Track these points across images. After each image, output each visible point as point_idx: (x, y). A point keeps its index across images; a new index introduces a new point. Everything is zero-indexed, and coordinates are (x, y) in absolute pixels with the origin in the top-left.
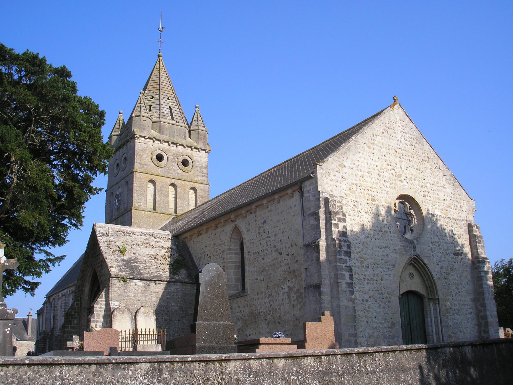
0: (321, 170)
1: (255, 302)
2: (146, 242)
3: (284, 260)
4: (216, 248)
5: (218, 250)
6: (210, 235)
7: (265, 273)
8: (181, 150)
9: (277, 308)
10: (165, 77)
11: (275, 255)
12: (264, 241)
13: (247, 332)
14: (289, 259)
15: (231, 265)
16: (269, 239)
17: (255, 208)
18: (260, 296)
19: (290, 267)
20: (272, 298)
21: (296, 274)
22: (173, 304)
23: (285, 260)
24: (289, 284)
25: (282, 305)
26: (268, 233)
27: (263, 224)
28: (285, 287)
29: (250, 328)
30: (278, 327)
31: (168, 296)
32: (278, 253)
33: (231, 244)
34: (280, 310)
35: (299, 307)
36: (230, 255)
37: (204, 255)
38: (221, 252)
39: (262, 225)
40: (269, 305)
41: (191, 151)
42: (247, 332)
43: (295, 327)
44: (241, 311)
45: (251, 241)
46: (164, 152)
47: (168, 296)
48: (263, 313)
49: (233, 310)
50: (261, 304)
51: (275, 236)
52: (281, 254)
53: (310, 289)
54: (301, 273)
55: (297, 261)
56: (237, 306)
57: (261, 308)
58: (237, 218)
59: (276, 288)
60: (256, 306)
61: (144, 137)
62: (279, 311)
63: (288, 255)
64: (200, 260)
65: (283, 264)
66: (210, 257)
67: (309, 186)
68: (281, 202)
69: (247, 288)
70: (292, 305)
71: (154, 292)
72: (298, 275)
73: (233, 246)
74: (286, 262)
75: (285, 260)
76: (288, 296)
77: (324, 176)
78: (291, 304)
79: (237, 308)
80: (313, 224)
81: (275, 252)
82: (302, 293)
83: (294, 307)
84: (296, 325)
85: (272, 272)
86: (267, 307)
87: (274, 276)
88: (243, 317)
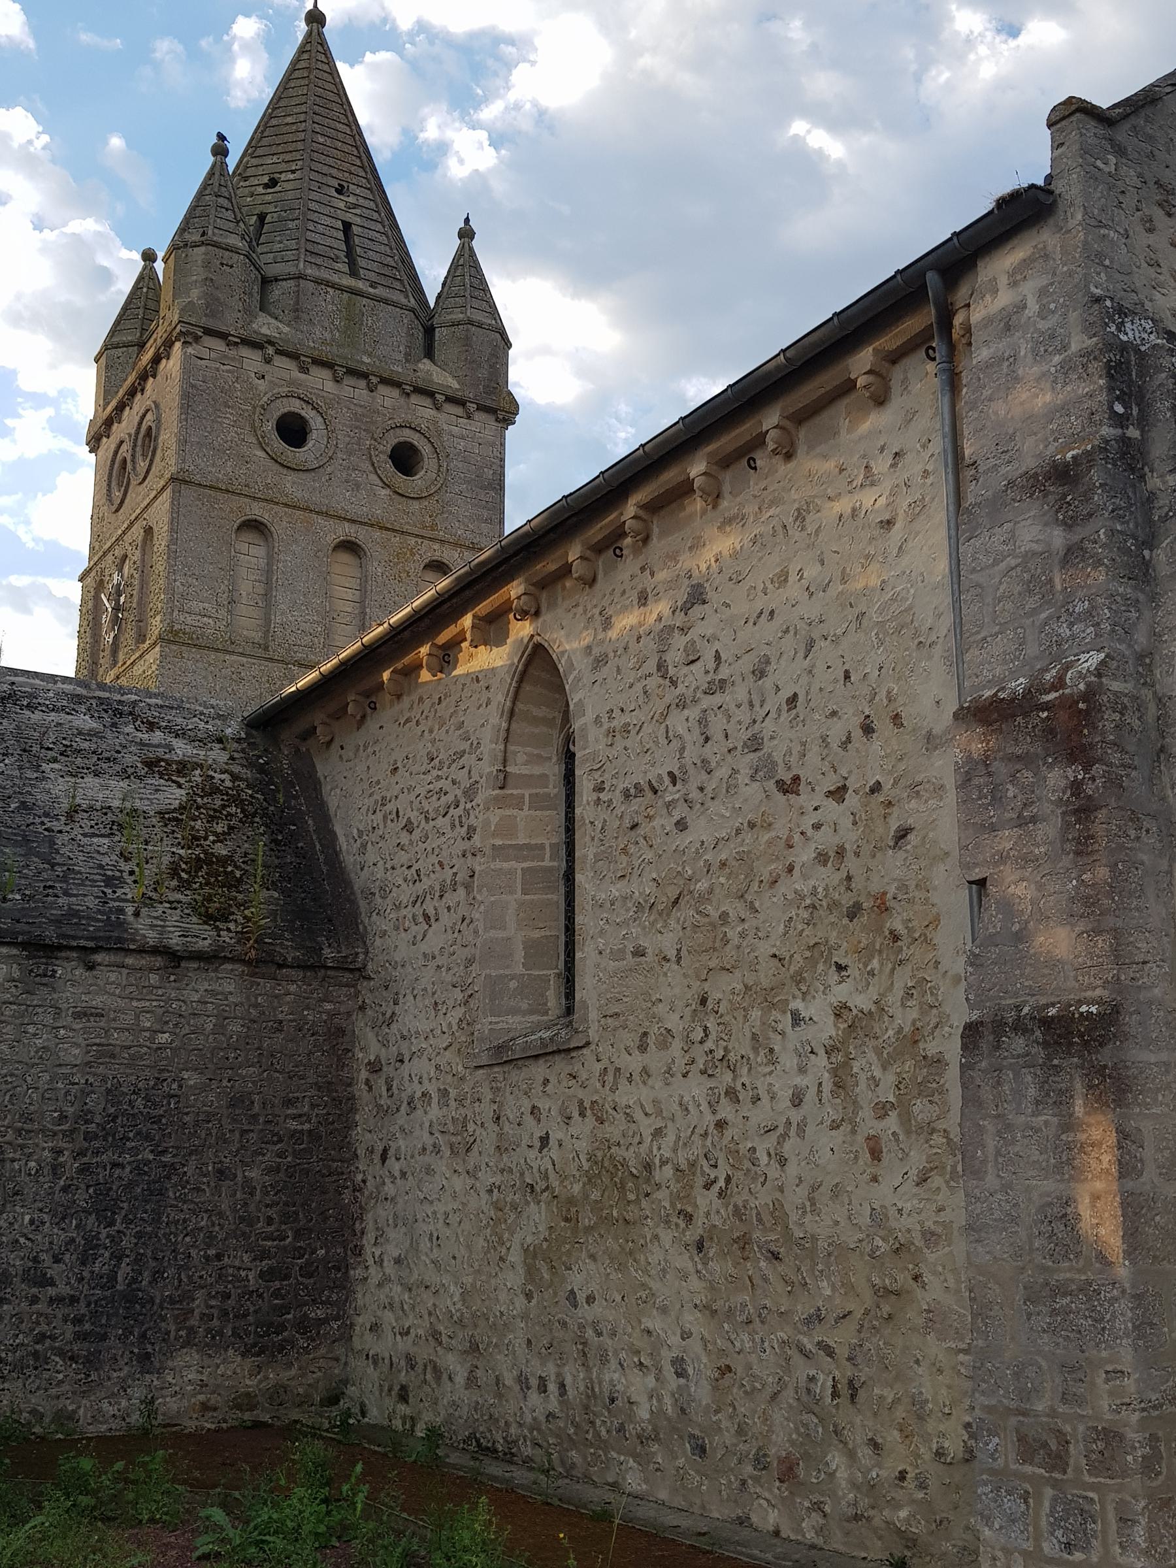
0: (1112, 159)
1: (626, 1095)
2: (86, 745)
3: (810, 832)
4: (439, 778)
5: (444, 784)
6: (411, 708)
7: (686, 912)
8: (388, 403)
9: (764, 1146)
10: (346, 148)
11: (751, 792)
12: (686, 712)
13: (575, 1280)
14: (846, 822)
15: (505, 865)
16: (717, 699)
17: (641, 513)
18: (655, 1059)
19: (849, 878)
20: (728, 1077)
21: (899, 927)
22: (192, 1078)
23: (817, 827)
24: (842, 992)
25: (792, 1133)
26: (711, 665)
27: (686, 609)
28: (817, 1009)
29: (593, 1257)
30: (766, 1279)
31: (164, 1038)
32: (771, 785)
33: (511, 748)
34: (783, 1162)
35: (917, 1159)
36: (508, 812)
37: (385, 817)
38: (459, 792)
39: (680, 619)
40: (709, 1119)
41: (433, 412)
42: (575, 1280)
43: (886, 1309)
44: (545, 1140)
45: (615, 723)
46: (314, 408)
47: (164, 1038)
48: (668, 1171)
49: (507, 1128)
50: (660, 1113)
51: (760, 673)
52: (789, 787)
53: (1019, 1044)
54: (936, 921)
55: (903, 834)
56: (526, 1106)
57: (658, 1133)
58: (544, 596)
59: (756, 1014)
60: (630, 1119)
61: (223, 336)
62: (774, 1171)
63: (838, 794)
64: (364, 846)
65: (804, 855)
66: (409, 828)
67: (1014, 284)
68: (801, 450)
69: (585, 1007)
70: (860, 1138)
71: (77, 1016)
72: (910, 930)
73: (521, 758)
74: (825, 839)
75: (817, 827)
76: (835, 1072)
77: (1129, 201)
78: (854, 1132)
79: (529, 1120)
80: (1037, 548)
81: (753, 778)
82: (938, 1062)
83: (876, 1154)
84: (897, 1294)
85: (735, 908)
86: (695, 1138)
87: (743, 935)
88: (554, 1182)
